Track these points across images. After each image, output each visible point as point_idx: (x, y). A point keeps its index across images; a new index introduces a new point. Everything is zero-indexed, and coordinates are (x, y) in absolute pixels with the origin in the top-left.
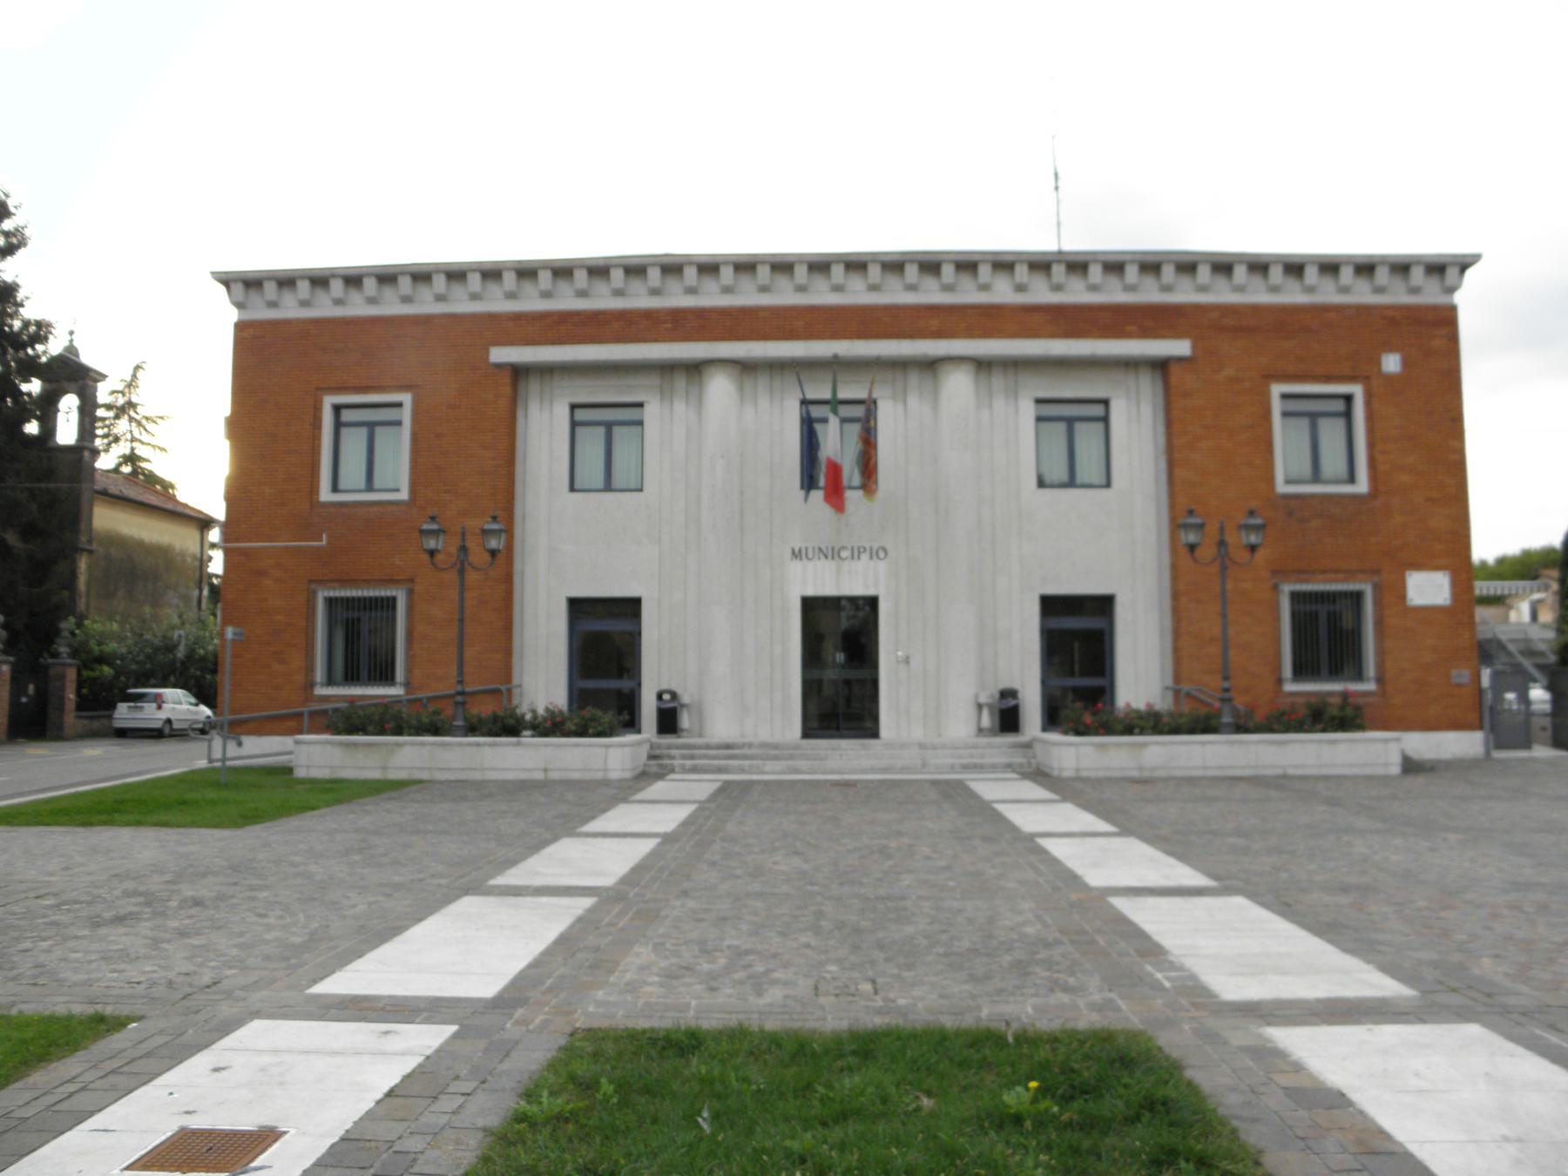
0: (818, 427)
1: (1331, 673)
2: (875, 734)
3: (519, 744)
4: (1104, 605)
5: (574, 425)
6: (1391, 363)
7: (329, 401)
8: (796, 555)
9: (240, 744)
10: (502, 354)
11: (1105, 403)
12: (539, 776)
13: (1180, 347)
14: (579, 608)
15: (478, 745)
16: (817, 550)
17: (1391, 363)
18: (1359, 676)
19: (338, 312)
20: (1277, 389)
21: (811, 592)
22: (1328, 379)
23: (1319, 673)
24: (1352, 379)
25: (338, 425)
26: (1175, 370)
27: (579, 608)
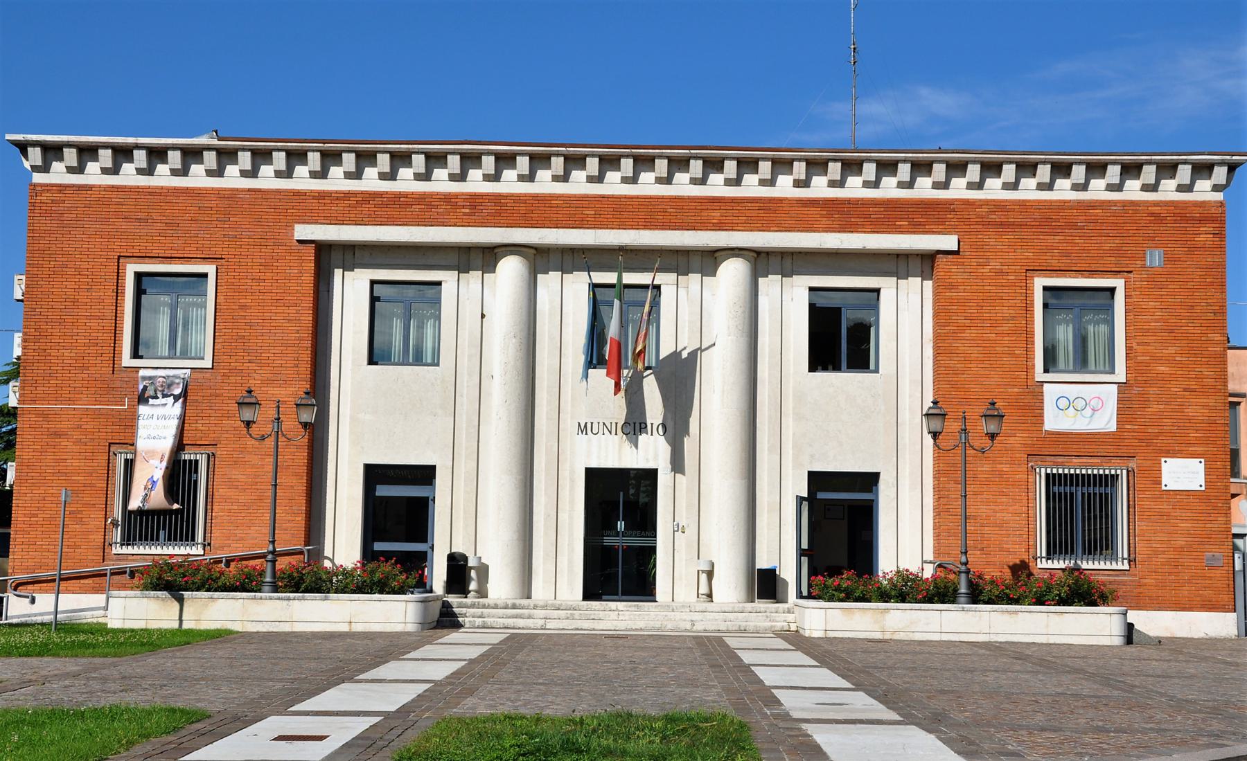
0: (603, 309)
1: (822, 370)
2: (809, 371)
3: (326, 599)
4: (870, 480)
5: (374, 300)
6: (1155, 258)
7: (131, 269)
8: (583, 429)
9: (33, 601)
10: (304, 231)
11: (878, 291)
12: (344, 628)
13: (948, 242)
14: (375, 475)
15: (289, 599)
16: (601, 425)
17: (1155, 258)
18: (1114, 557)
19: (144, 181)
20: (1040, 282)
21: (594, 464)
22: (1092, 273)
23: (827, 370)
24: (1116, 273)
25: (139, 292)
26: (526, 597)
27: (375, 475)
